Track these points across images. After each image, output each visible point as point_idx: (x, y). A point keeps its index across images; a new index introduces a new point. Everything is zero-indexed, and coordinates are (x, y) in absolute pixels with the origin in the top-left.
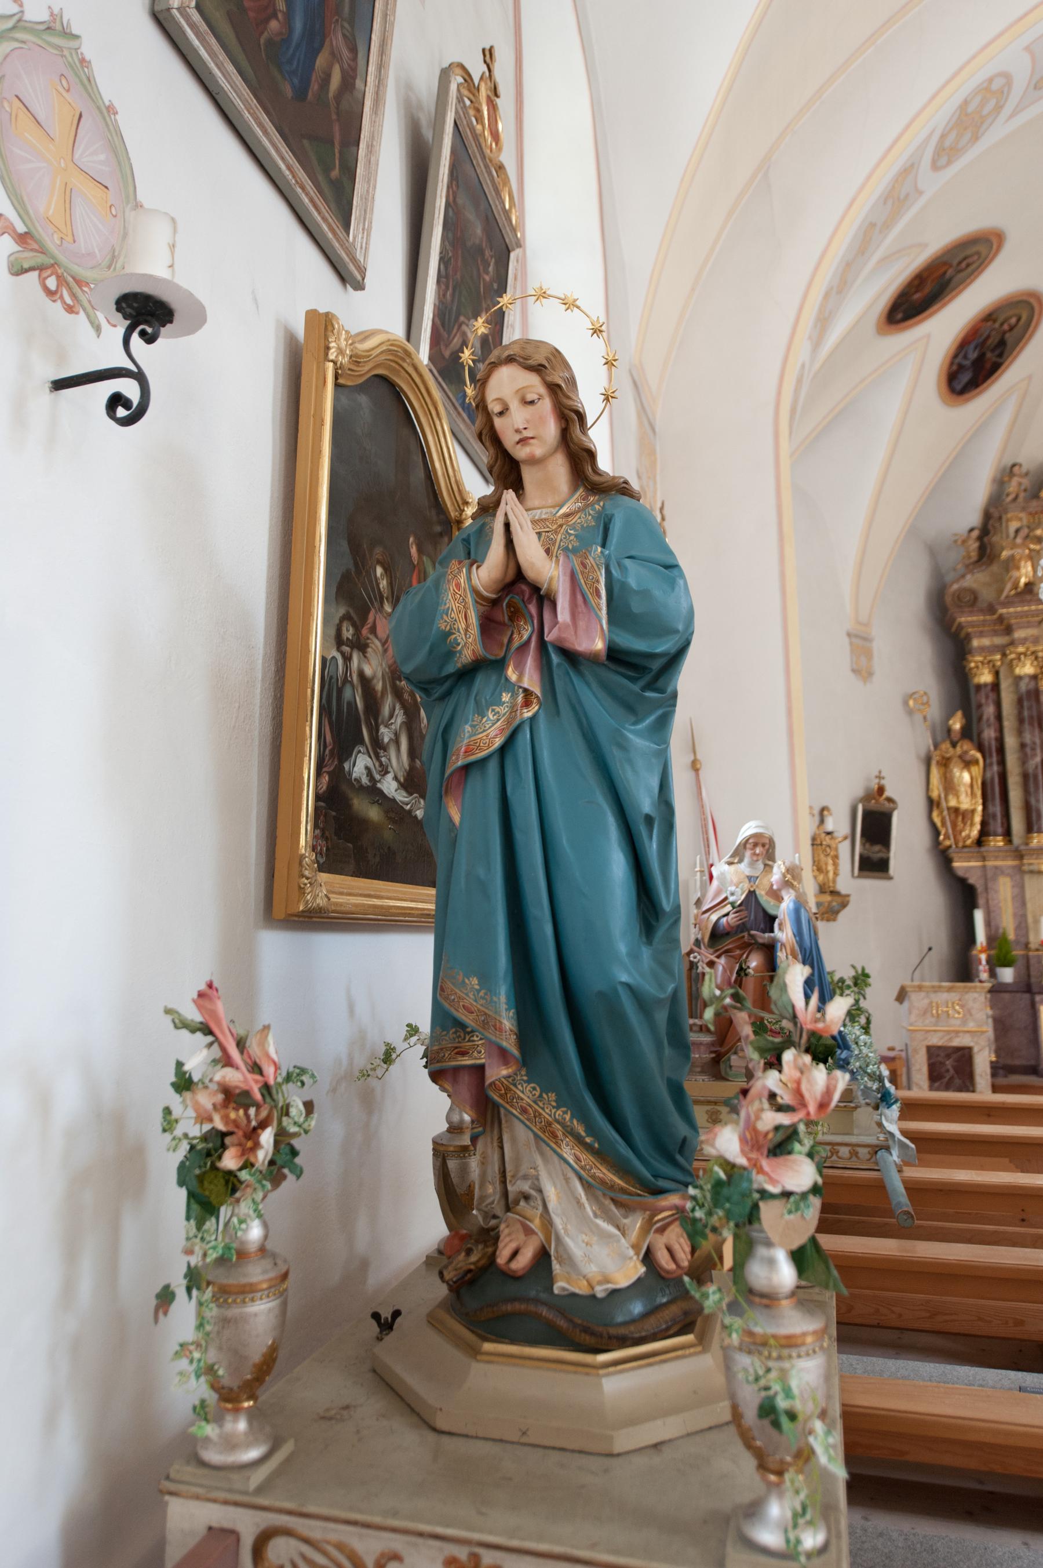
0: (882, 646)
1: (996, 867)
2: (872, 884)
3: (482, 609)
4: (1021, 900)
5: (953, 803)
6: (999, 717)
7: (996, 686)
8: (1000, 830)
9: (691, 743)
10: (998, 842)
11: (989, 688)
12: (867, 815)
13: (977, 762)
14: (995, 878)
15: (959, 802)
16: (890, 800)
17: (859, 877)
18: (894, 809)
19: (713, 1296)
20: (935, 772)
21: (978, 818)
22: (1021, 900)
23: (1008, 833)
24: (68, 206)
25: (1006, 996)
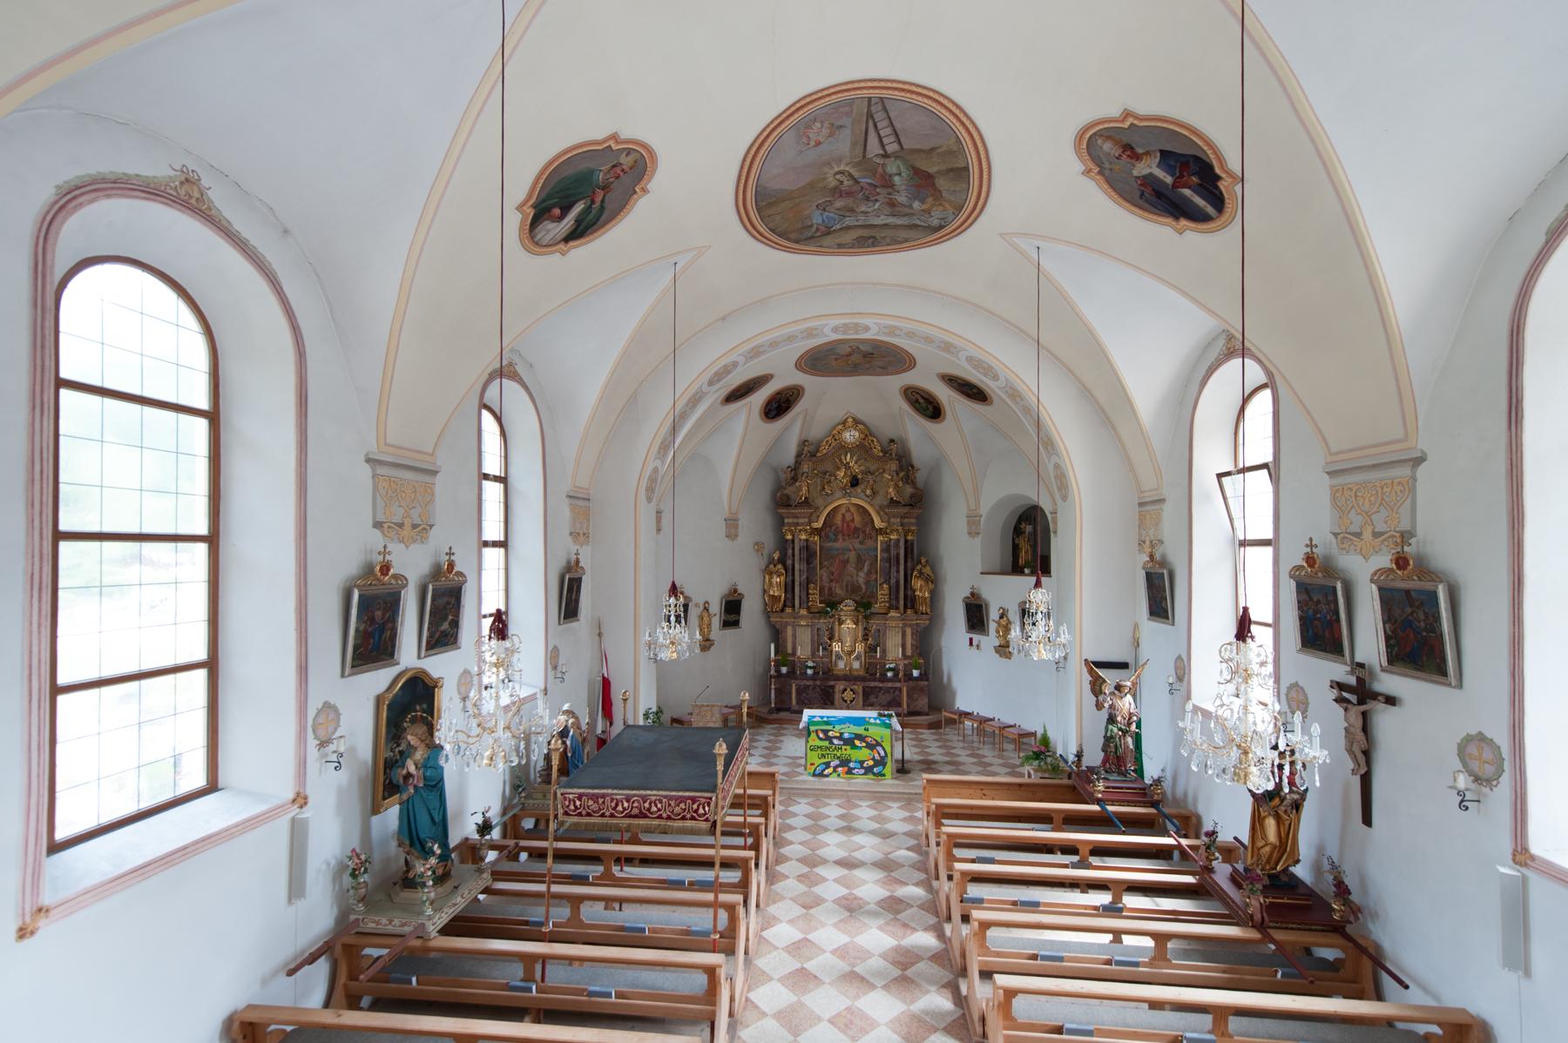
0: (744, 522)
4: (794, 635)
22: (794, 635)
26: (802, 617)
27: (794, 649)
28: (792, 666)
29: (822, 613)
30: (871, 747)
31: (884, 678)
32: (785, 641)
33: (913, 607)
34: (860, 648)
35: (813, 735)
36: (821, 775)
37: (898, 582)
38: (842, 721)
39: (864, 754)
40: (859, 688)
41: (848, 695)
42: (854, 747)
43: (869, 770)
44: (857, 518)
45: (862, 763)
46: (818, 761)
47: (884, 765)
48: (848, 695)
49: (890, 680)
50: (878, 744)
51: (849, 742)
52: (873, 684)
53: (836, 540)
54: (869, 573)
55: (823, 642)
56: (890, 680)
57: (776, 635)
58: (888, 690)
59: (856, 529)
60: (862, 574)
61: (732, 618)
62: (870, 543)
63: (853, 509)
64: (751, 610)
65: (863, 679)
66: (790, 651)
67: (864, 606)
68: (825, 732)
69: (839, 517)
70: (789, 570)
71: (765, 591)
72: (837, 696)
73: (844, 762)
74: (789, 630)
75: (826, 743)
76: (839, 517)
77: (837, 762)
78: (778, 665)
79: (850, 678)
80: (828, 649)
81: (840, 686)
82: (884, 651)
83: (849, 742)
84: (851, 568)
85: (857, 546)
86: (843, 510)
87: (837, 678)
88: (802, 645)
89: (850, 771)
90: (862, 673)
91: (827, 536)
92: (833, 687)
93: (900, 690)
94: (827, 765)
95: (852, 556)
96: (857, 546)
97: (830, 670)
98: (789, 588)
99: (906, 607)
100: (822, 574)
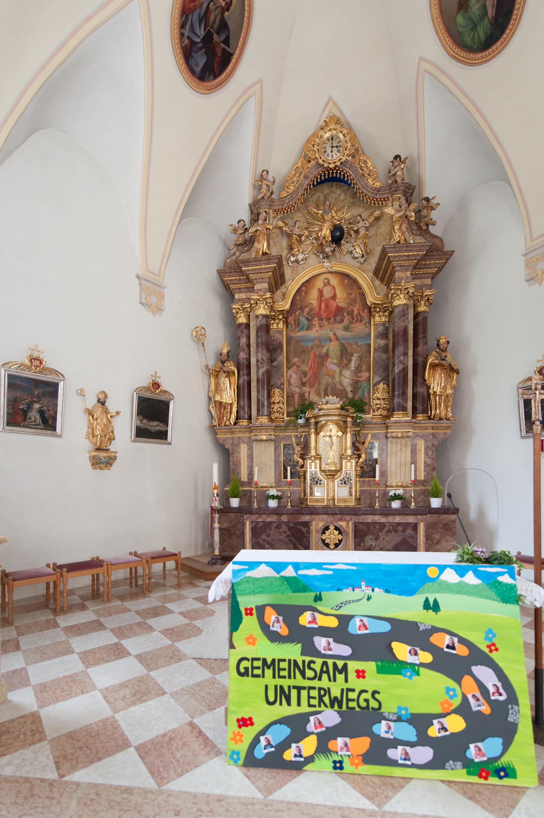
0: (174, 292)
1: (239, 438)
2: (150, 448)
3: (425, 473)
4: (250, 457)
5: (218, 398)
6: (249, 346)
7: (248, 326)
8: (246, 416)
9: (209, 413)
10: (245, 423)
11: (244, 326)
12: (139, 398)
13: (233, 372)
14: (238, 445)
15: (221, 398)
16: (165, 392)
17: (134, 441)
18: (171, 400)
19: (89, 730)
20: (213, 380)
21: (235, 409)
22: (250, 457)
23: (250, 418)
24: (165, 260)
25: (232, 515)
26: (261, 428)
27: (251, 474)
28: (246, 497)
29: (291, 425)
30: (453, 664)
31: (387, 512)
32: (238, 464)
33: (425, 411)
34: (350, 467)
35: (250, 623)
36: (275, 761)
37: (405, 369)
38: (343, 579)
39: (426, 690)
40: (348, 525)
41: (332, 536)
42: (390, 664)
43: (447, 752)
44: (341, 294)
45: (421, 722)
46: (264, 714)
47: (508, 734)
48: (332, 536)
49: (397, 512)
50: (478, 657)
51: (375, 648)
52: (370, 519)
53: (309, 328)
54: (358, 370)
55: (292, 468)
56: (397, 512)
57: (227, 455)
58: (395, 528)
59: (339, 310)
60: (347, 373)
61: (154, 426)
62: (359, 328)
63: (334, 281)
64: (188, 418)
65: (353, 512)
66: (244, 477)
67: (355, 407)
68: (289, 613)
69: (314, 294)
70: (244, 367)
71: (210, 399)
72: (314, 538)
73: (359, 719)
74: (244, 449)
75: (293, 651)
76: (314, 294)
77: (330, 717)
78: (225, 497)
79: (333, 511)
80: (299, 474)
81: (317, 524)
82: (383, 474)
83: (375, 648)
84: (331, 365)
85: (341, 333)
86: (319, 283)
87: (314, 511)
88: (262, 466)
89: (377, 754)
90: (352, 503)
91: (298, 323)
92: (307, 524)
93: (415, 527)
94: (297, 726)
95: (333, 348)
96: (341, 333)
97: (303, 501)
98: (244, 392)
99: (414, 409)
100: (291, 377)
